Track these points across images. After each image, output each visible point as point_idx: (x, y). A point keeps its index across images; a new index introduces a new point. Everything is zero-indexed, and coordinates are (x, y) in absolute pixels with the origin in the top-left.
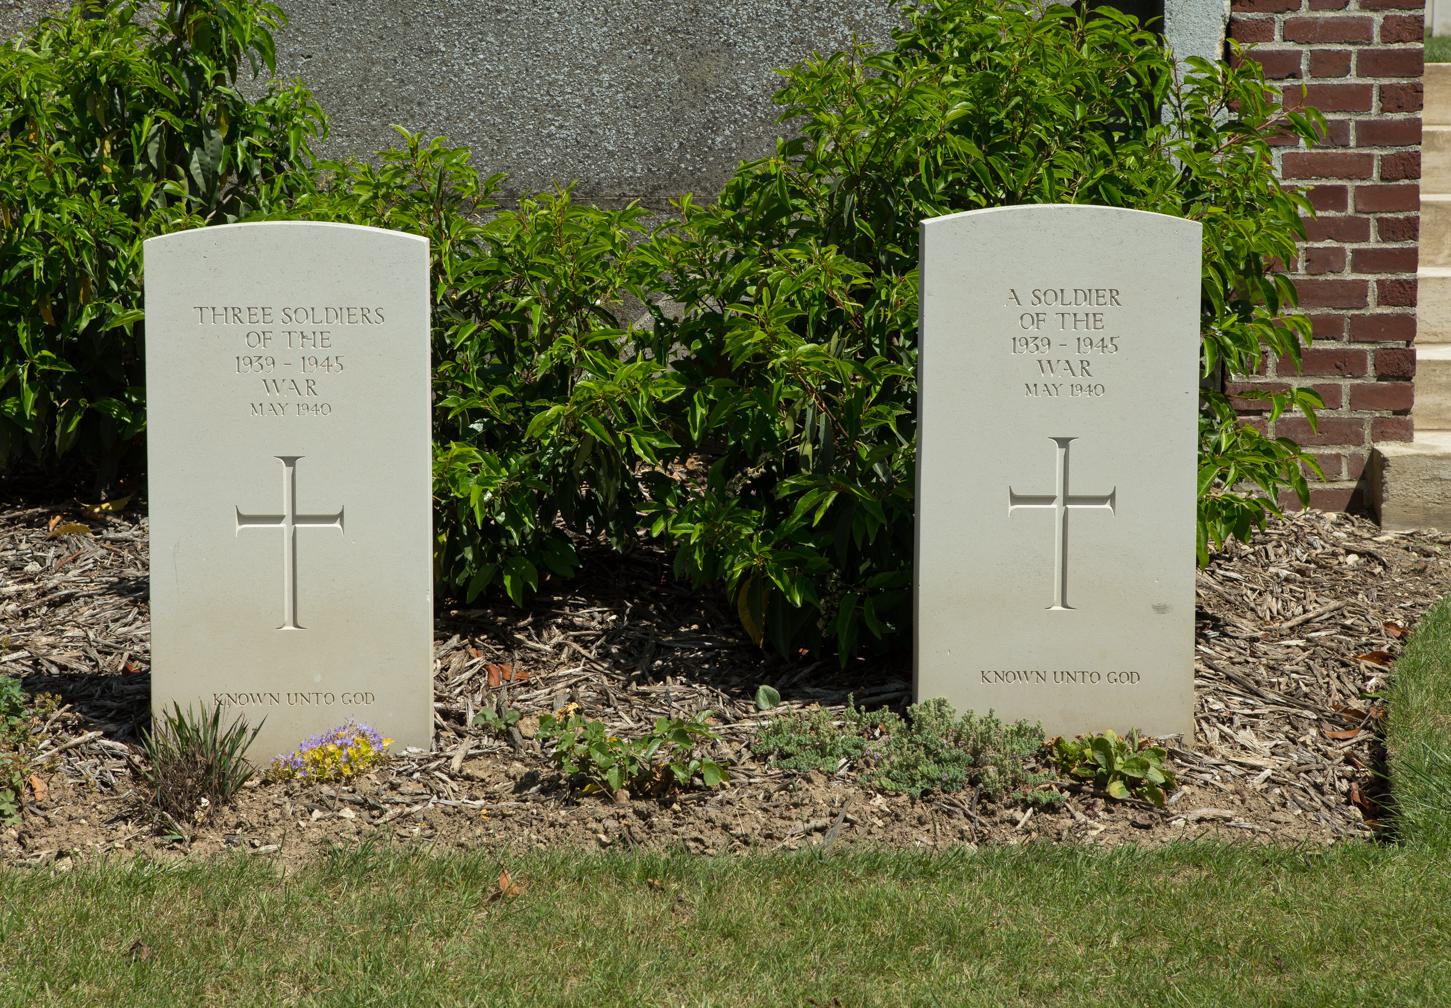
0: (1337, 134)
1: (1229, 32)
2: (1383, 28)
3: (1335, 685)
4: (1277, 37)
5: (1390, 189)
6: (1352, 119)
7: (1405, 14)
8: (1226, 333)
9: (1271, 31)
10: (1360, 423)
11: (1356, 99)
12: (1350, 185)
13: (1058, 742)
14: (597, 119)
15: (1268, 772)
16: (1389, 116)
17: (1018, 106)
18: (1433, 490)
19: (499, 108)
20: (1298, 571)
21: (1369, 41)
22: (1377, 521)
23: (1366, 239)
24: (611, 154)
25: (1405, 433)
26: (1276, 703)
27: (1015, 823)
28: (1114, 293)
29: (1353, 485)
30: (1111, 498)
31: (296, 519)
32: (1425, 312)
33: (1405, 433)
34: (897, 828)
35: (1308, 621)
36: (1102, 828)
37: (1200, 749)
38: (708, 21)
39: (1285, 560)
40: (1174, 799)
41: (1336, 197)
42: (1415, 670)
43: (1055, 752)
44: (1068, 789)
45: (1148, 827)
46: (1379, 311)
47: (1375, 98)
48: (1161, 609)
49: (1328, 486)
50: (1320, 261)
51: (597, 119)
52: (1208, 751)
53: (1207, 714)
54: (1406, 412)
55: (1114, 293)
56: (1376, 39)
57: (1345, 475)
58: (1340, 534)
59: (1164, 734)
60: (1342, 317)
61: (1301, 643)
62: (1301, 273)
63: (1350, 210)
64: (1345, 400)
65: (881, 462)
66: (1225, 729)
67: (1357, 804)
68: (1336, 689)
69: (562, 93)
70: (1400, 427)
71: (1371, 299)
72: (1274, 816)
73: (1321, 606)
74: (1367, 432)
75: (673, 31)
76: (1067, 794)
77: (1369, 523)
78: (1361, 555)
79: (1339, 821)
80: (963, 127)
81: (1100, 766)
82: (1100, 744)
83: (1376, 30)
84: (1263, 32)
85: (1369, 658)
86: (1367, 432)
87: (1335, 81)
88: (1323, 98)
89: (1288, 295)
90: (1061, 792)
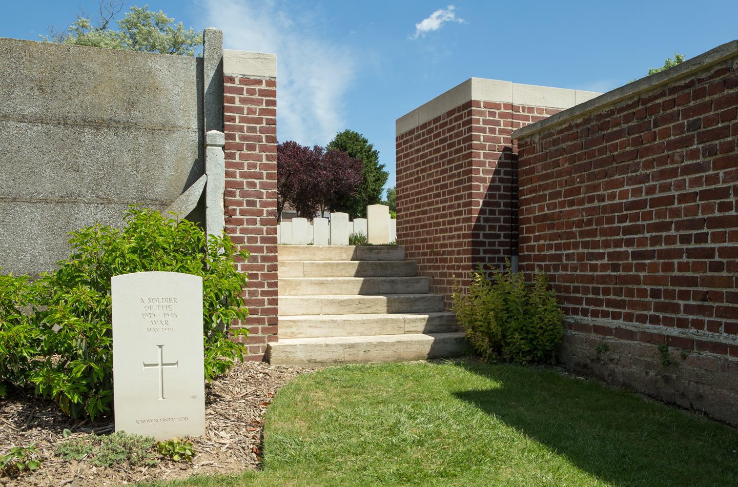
0: (255, 259)
1: (225, 230)
2: (266, 231)
3: (252, 413)
4: (238, 232)
5: (270, 274)
6: (259, 255)
7: (272, 227)
8: (221, 313)
9: (236, 231)
10: (264, 337)
11: (260, 250)
12: (259, 273)
13: (158, 443)
14: (37, 254)
15: (227, 445)
16: (269, 254)
17: (151, 245)
18: (284, 354)
19: (4, 250)
20: (246, 379)
21: (263, 234)
22: (269, 364)
23: (264, 287)
24: (42, 264)
25: (276, 340)
26: (234, 421)
27: (141, 472)
28: (175, 299)
29: (263, 354)
30: (145, 365)
31: (163, 365)
32: (281, 307)
33: (276, 340)
34: (98, 479)
35: (247, 394)
36: (170, 471)
37: (208, 439)
38: (72, 225)
39: (242, 376)
40: (195, 458)
41: (255, 276)
42: (274, 408)
43: (158, 446)
44: (160, 459)
45: (185, 470)
46: (268, 307)
47: (265, 249)
48: (194, 397)
49: (256, 355)
50: (252, 294)
51: (37, 254)
52: (210, 440)
53: (211, 427)
54: (276, 334)
55: (175, 299)
56: (265, 233)
57: (261, 351)
58: (259, 368)
59: (195, 435)
60: (258, 309)
61: (244, 401)
62: (247, 297)
63: (260, 280)
64: (260, 331)
65: (105, 354)
66: (216, 432)
67: (255, 453)
68: (251, 415)
69: (25, 246)
70: (274, 337)
71: (266, 303)
72: (227, 461)
73: (251, 389)
74: (266, 340)
75: (61, 228)
76: (160, 460)
77: (267, 364)
78: (264, 374)
79: (249, 459)
80: (134, 251)
81: (171, 450)
82: (171, 443)
83: (264, 231)
84: (234, 231)
85: (263, 404)
86: (266, 340)
87: (254, 245)
88: (251, 249)
89: (242, 302)
90: (158, 460)
